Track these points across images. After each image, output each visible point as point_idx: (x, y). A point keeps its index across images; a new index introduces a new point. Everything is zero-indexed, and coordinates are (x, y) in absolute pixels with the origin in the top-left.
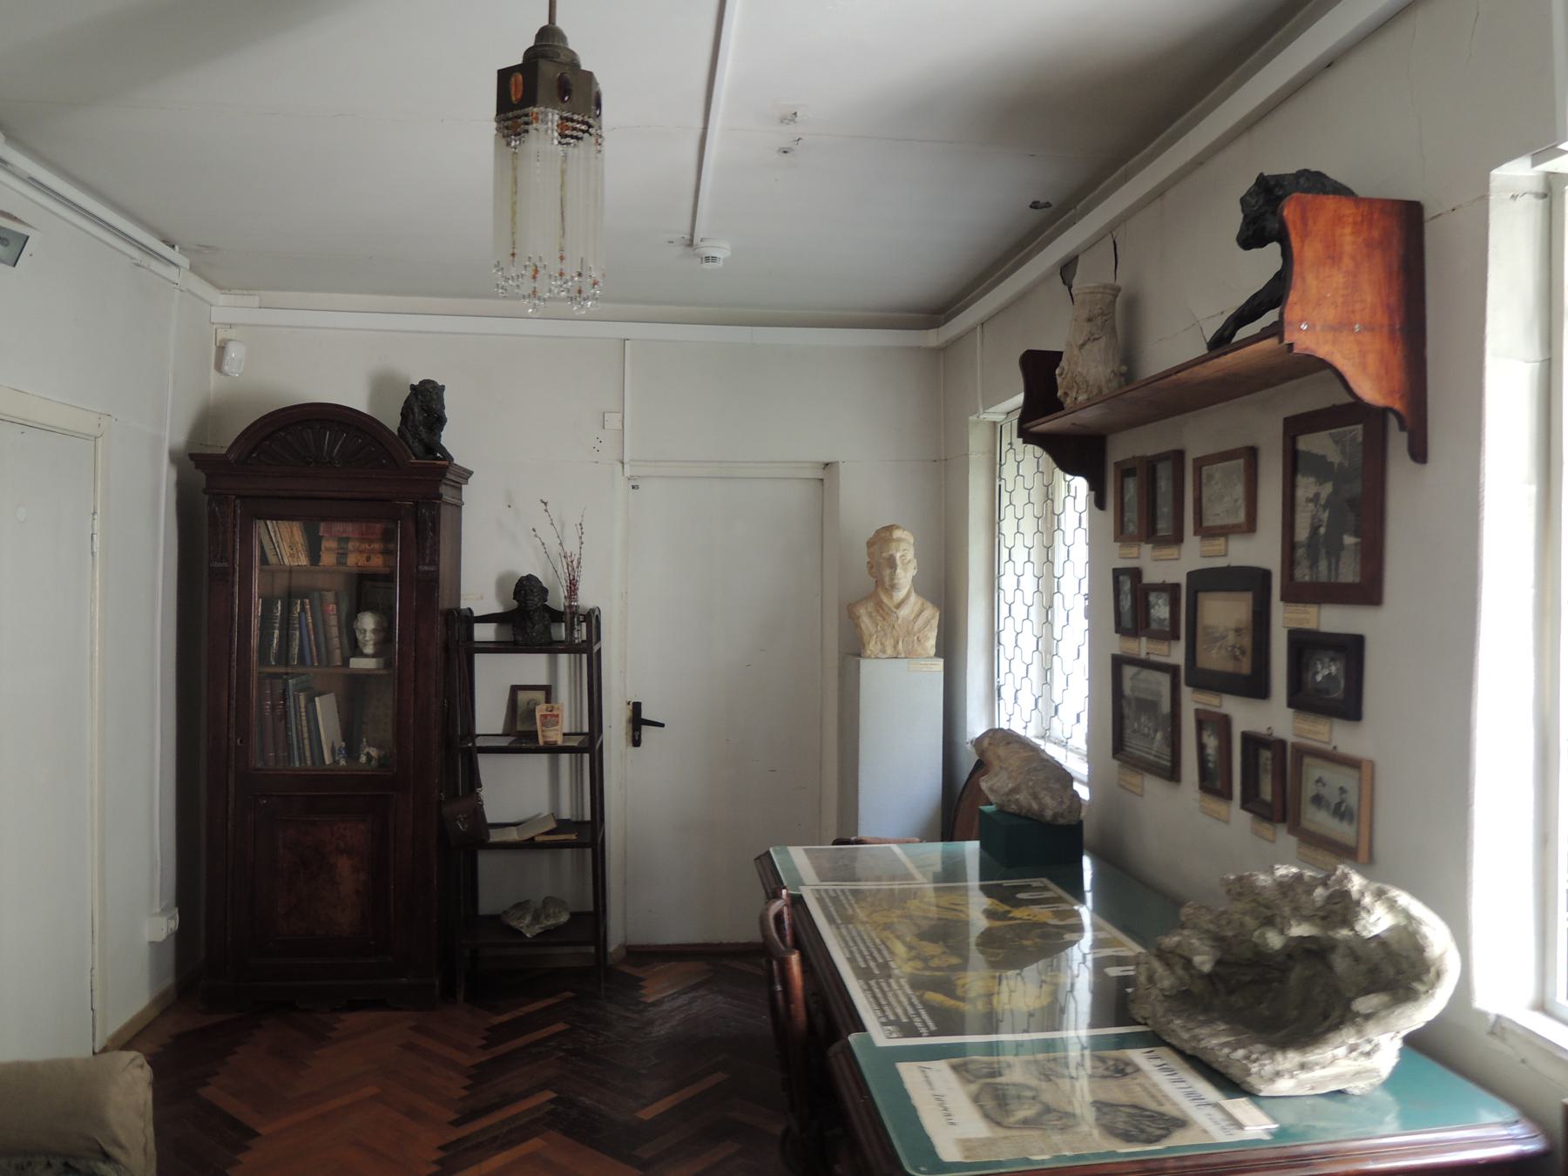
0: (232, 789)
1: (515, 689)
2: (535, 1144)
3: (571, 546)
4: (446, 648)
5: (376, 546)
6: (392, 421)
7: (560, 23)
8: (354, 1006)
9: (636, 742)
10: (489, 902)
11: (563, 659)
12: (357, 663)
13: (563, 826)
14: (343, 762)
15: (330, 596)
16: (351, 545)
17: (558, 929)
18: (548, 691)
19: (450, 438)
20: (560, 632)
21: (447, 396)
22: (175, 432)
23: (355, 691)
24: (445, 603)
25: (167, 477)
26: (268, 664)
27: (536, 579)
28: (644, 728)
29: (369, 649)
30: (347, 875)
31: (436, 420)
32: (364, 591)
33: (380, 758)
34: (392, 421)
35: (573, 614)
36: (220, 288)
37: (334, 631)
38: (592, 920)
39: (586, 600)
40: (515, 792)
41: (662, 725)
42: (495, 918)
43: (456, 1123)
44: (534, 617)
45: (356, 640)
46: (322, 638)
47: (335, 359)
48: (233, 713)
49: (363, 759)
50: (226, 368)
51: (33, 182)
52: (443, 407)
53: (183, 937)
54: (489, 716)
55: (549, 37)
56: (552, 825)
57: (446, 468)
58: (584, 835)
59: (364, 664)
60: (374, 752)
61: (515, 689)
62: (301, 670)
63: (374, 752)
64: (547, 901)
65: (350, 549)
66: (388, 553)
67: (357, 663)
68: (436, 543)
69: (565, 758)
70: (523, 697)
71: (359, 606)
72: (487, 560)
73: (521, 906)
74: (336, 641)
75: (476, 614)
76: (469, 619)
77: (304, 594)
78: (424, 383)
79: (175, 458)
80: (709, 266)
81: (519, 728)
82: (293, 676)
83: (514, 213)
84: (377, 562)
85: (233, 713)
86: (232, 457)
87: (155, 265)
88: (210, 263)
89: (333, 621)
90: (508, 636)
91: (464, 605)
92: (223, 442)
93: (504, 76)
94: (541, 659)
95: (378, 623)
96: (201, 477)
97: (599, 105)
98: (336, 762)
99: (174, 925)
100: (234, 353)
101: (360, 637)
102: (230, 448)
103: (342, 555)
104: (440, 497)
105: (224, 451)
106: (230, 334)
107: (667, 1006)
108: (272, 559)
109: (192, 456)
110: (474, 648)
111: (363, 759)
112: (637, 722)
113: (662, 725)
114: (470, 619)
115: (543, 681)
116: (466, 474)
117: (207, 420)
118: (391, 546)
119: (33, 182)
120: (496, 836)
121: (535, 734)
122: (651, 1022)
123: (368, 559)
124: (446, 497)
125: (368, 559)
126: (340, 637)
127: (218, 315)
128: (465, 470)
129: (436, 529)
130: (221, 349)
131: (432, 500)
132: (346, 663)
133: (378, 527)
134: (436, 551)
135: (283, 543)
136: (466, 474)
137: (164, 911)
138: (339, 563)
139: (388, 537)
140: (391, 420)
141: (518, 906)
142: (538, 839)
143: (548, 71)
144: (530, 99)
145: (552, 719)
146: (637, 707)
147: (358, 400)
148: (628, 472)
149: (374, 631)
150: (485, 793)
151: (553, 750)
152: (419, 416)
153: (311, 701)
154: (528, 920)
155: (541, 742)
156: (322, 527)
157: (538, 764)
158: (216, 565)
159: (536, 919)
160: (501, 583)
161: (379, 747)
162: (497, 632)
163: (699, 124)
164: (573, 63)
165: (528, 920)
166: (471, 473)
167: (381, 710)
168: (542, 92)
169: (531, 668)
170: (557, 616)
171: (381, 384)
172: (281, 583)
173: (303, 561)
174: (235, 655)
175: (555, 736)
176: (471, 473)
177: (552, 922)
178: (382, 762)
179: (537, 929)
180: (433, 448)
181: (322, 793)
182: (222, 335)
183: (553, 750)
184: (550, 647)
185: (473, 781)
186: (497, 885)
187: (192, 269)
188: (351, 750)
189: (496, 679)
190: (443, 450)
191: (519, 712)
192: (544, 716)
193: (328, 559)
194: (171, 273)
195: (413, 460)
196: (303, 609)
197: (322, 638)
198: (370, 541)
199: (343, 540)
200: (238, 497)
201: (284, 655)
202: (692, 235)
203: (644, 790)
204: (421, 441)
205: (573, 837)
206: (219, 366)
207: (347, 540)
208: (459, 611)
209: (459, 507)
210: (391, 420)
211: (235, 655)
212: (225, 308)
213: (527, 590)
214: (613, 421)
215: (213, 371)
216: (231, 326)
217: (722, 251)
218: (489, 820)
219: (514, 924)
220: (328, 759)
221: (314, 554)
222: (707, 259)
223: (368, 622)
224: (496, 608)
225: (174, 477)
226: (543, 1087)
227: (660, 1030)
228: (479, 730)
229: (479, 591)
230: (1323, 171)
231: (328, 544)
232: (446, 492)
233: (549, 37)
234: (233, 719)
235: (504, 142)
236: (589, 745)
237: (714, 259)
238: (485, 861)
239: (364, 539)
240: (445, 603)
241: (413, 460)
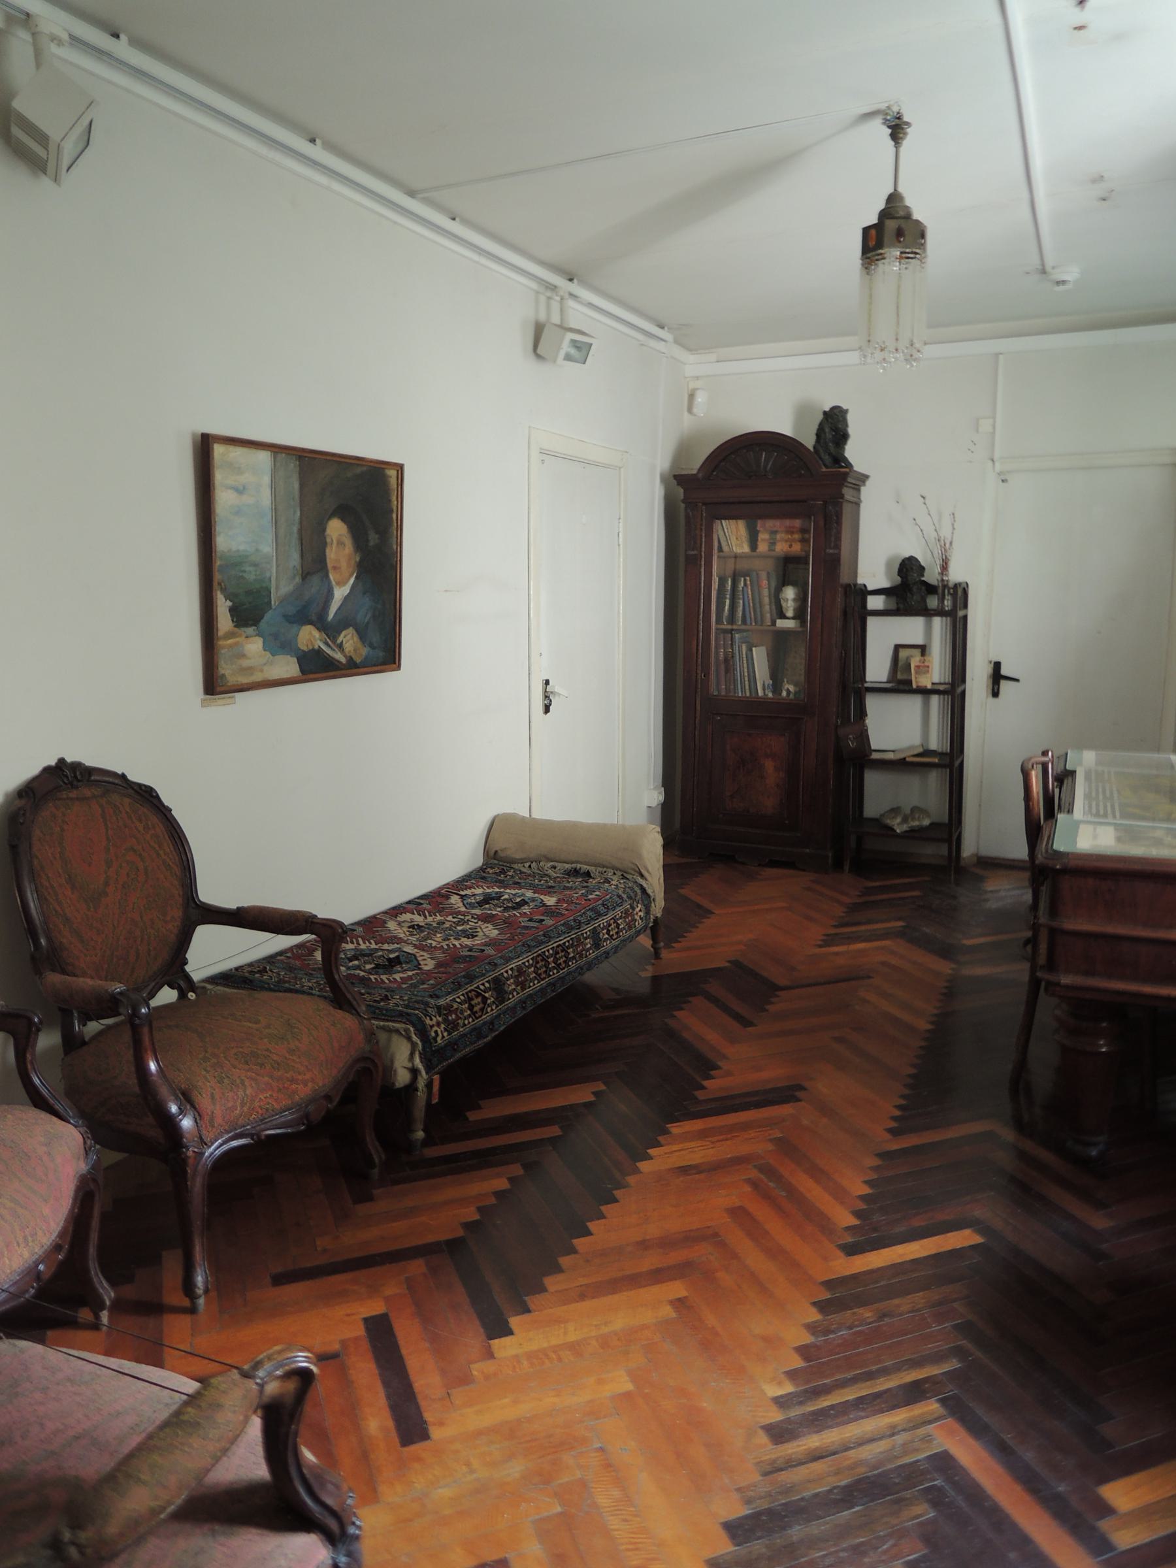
0: (698, 708)
1: (897, 648)
2: (887, 943)
3: (946, 532)
4: (845, 613)
5: (796, 536)
6: (809, 441)
7: (900, 189)
9: (995, 694)
10: (871, 809)
11: (937, 621)
12: (781, 624)
13: (927, 753)
14: (770, 695)
15: (763, 575)
16: (778, 537)
17: (921, 829)
18: (923, 649)
19: (853, 452)
20: (933, 602)
21: (850, 418)
22: (662, 462)
23: (780, 644)
24: (845, 579)
25: (658, 492)
27: (916, 560)
28: (1003, 683)
29: (790, 614)
30: (772, 774)
31: (841, 437)
32: (788, 569)
33: (796, 693)
34: (809, 441)
35: (945, 586)
36: (689, 349)
37: (766, 600)
38: (951, 827)
39: (955, 575)
40: (895, 726)
41: (1017, 680)
42: (876, 821)
43: (835, 926)
44: (914, 589)
45: (781, 607)
46: (758, 605)
47: (771, 404)
49: (784, 694)
50: (695, 410)
51: (590, 305)
52: (847, 426)
53: (667, 808)
54: (877, 669)
55: (894, 199)
56: (921, 750)
57: (846, 475)
58: (949, 761)
59: (788, 624)
60: (792, 688)
61: (897, 648)
62: (743, 627)
63: (792, 688)
64: (914, 809)
65: (779, 539)
66: (804, 541)
67: (781, 624)
68: (839, 532)
69: (935, 700)
70: (903, 654)
71: (784, 581)
72: (877, 549)
73: (895, 811)
74: (767, 608)
75: (870, 588)
76: (864, 592)
77: (746, 574)
78: (833, 408)
79: (664, 480)
80: (1061, 288)
81: (900, 676)
82: (739, 631)
83: (870, 315)
84: (797, 548)
86: (700, 475)
87: (653, 343)
88: (688, 336)
89: (766, 592)
90: (893, 606)
91: (860, 581)
92: (694, 465)
93: (866, 231)
94: (918, 622)
95: (796, 594)
97: (923, 236)
99: (661, 798)
100: (700, 399)
101: (784, 604)
102: (699, 470)
103: (773, 544)
104: (842, 496)
105: (695, 472)
106: (698, 384)
107: (1003, 894)
108: (725, 548)
109: (675, 477)
110: (864, 614)
111: (784, 694)
112: (997, 676)
113: (1017, 680)
114: (864, 592)
115: (920, 642)
116: (864, 478)
117: (683, 450)
118: (806, 536)
119: (590, 305)
120: (875, 756)
121: (910, 682)
122: (987, 900)
123: (791, 546)
124: (847, 497)
125: (791, 546)
126: (770, 604)
127: (689, 371)
128: (863, 475)
129: (839, 523)
130: (692, 396)
131: (836, 500)
132: (774, 623)
133: (797, 523)
134: (838, 538)
135: (732, 536)
136: (864, 478)
137: (655, 788)
138: (770, 550)
139: (804, 531)
140: (808, 440)
141: (892, 810)
143: (891, 225)
144: (880, 244)
145: (924, 669)
146: (997, 666)
147: (784, 426)
148: (998, 467)
149: (794, 600)
150: (869, 721)
151: (925, 692)
152: (829, 435)
154: (899, 820)
155: (914, 686)
156: (759, 523)
157: (914, 704)
159: (905, 820)
160: (889, 564)
161: (795, 685)
162: (885, 602)
163: (1025, 195)
164: (908, 216)
165: (899, 820)
166: (867, 477)
167: (797, 661)
168: (886, 240)
169: (910, 629)
170: (931, 589)
171: (802, 412)
172: (730, 566)
173: (746, 549)
175: (926, 682)
176: (867, 477)
177: (916, 823)
179: (905, 827)
180: (839, 460)
181: (759, 715)
182: (692, 385)
184: (926, 612)
185: (862, 713)
186: (880, 795)
187: (676, 342)
188: (776, 686)
189: (884, 637)
190: (846, 460)
191: (900, 664)
192: (918, 667)
193: (763, 547)
194: (660, 346)
195: (824, 469)
196: (745, 584)
197: (758, 605)
198: (792, 533)
199: (774, 533)
200: (704, 504)
201: (732, 619)
202: (1043, 265)
203: (999, 737)
204: (830, 454)
205: (936, 760)
206: (690, 410)
207: (775, 532)
208: (855, 585)
209: (857, 504)
210: (808, 440)
212: (694, 365)
213: (908, 568)
214: (986, 426)
215: (686, 413)
216: (697, 378)
217: (1071, 274)
218: (873, 747)
219: (888, 822)
220: (760, 693)
221: (753, 545)
222: (1058, 283)
223: (789, 593)
224: (885, 583)
225: (662, 493)
226: (900, 919)
227: (993, 905)
228: (868, 679)
229: (873, 570)
230: (814, 431)
231: (763, 536)
232: (848, 493)
233: (894, 199)
235: (865, 272)
236: (953, 693)
237: (1064, 282)
238: (872, 779)
239: (790, 531)
240: (845, 579)
241: (824, 469)
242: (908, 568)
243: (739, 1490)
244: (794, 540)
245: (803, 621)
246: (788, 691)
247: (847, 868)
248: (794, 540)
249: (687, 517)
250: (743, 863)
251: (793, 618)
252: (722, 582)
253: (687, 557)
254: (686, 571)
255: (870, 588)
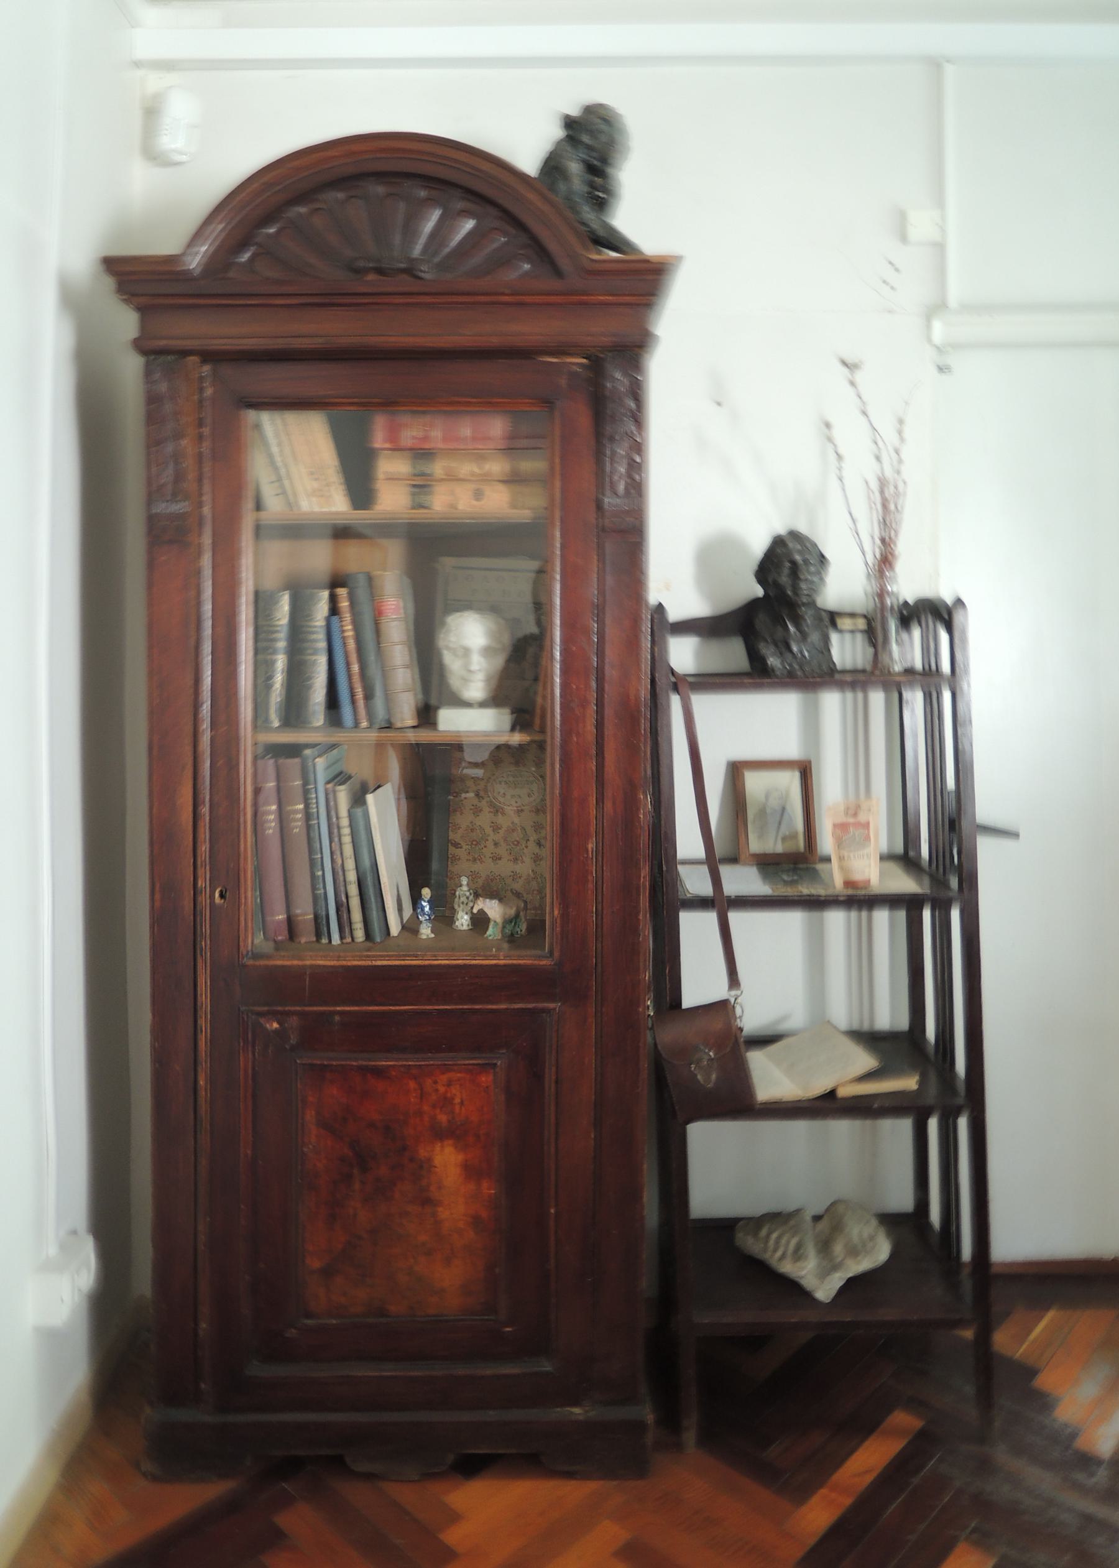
3: (889, 473)
8: (470, 1467)
11: (831, 702)
14: (426, 931)
23: (432, 780)
26: (268, 729)
29: (476, 690)
40: (777, 978)
41: (1013, 835)
48: (204, 833)
53: (107, 1304)
69: (882, 917)
70: (755, 783)
72: (701, 506)
85: (204, 833)
86: (195, 262)
96: (125, 322)
98: (410, 928)
111: (463, 921)
113: (1013, 835)
115: (792, 750)
123: (478, 495)
135: (294, 461)
142: (842, 1092)
149: (487, 651)
151: (860, 900)
153: (358, 800)
158: (161, 508)
162: (699, 655)
174: (206, 708)
178: (527, 930)
183: (860, 900)
193: (392, 500)
196: (334, 610)
211: (206, 708)
214: (922, 225)
219: (787, 1268)
221: (360, 484)
231: (391, 469)
234: (204, 848)
242: (786, 568)
243: (275, 941)
244: (486, 478)
245: (524, 715)
246: (480, 921)
247: (690, 1437)
248: (486, 478)
249: (153, 400)
250: (370, 1477)
251: (483, 705)
252: (263, 603)
253: (152, 521)
254: (151, 565)
255: (674, 614)
